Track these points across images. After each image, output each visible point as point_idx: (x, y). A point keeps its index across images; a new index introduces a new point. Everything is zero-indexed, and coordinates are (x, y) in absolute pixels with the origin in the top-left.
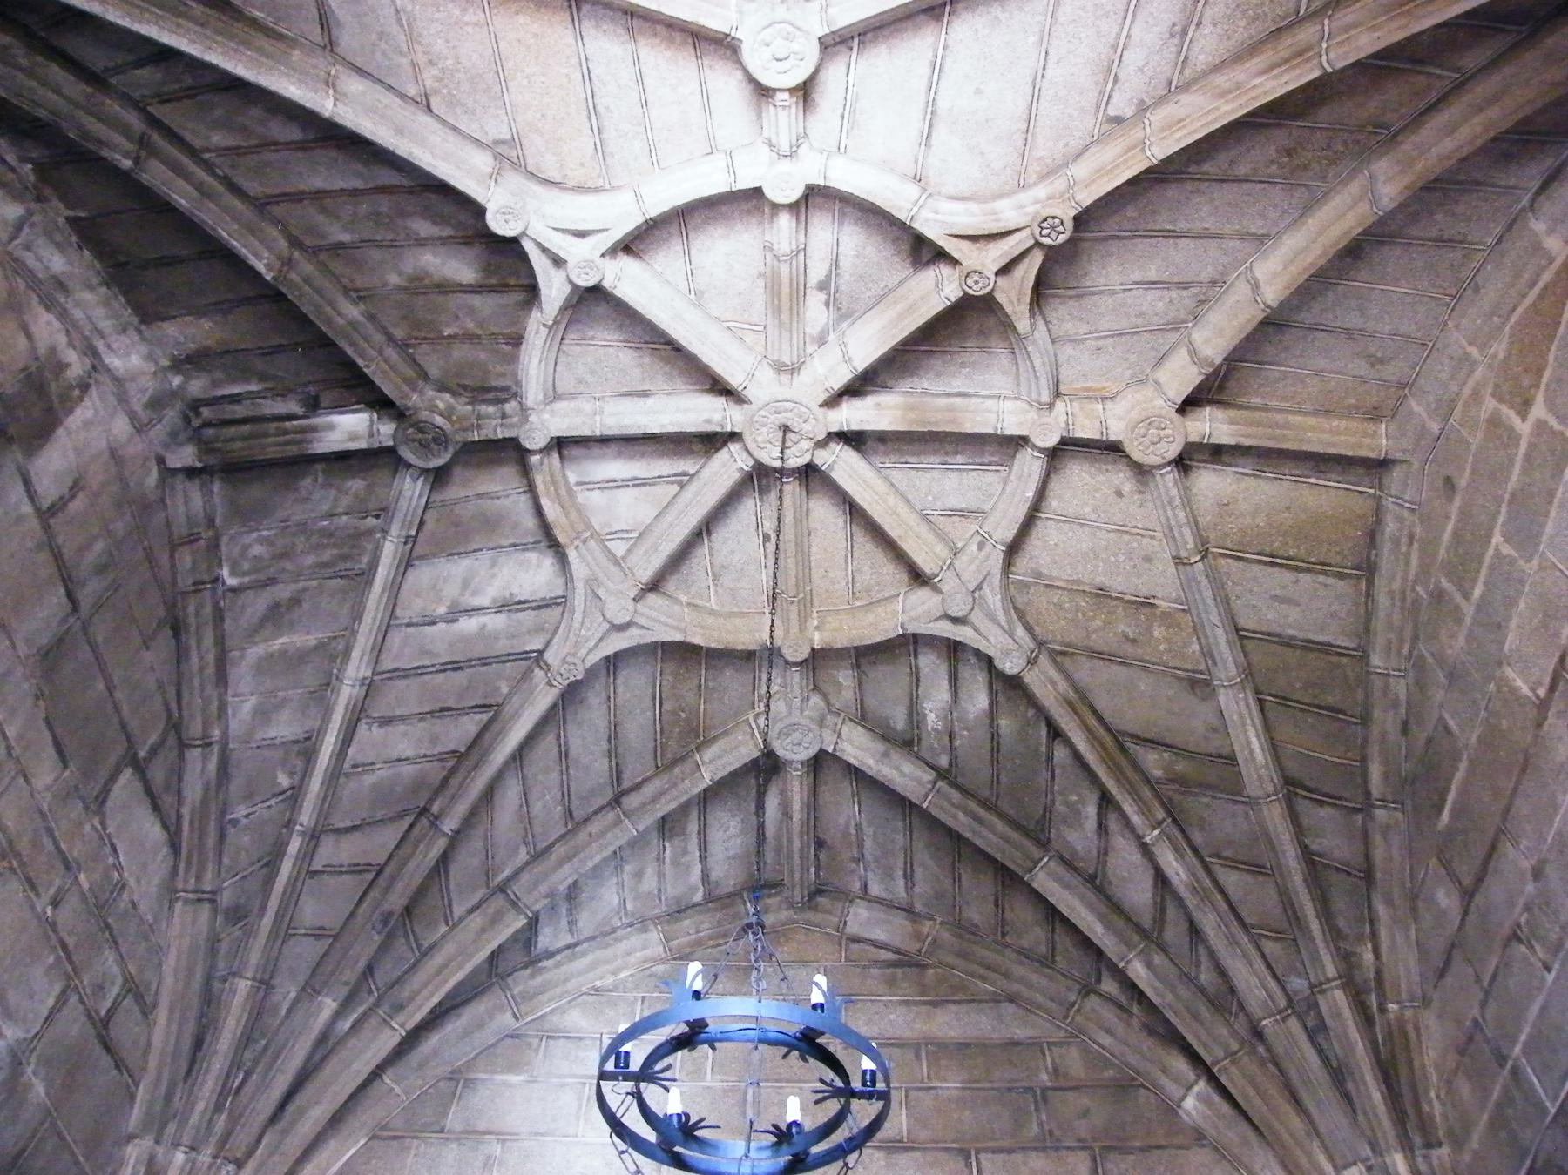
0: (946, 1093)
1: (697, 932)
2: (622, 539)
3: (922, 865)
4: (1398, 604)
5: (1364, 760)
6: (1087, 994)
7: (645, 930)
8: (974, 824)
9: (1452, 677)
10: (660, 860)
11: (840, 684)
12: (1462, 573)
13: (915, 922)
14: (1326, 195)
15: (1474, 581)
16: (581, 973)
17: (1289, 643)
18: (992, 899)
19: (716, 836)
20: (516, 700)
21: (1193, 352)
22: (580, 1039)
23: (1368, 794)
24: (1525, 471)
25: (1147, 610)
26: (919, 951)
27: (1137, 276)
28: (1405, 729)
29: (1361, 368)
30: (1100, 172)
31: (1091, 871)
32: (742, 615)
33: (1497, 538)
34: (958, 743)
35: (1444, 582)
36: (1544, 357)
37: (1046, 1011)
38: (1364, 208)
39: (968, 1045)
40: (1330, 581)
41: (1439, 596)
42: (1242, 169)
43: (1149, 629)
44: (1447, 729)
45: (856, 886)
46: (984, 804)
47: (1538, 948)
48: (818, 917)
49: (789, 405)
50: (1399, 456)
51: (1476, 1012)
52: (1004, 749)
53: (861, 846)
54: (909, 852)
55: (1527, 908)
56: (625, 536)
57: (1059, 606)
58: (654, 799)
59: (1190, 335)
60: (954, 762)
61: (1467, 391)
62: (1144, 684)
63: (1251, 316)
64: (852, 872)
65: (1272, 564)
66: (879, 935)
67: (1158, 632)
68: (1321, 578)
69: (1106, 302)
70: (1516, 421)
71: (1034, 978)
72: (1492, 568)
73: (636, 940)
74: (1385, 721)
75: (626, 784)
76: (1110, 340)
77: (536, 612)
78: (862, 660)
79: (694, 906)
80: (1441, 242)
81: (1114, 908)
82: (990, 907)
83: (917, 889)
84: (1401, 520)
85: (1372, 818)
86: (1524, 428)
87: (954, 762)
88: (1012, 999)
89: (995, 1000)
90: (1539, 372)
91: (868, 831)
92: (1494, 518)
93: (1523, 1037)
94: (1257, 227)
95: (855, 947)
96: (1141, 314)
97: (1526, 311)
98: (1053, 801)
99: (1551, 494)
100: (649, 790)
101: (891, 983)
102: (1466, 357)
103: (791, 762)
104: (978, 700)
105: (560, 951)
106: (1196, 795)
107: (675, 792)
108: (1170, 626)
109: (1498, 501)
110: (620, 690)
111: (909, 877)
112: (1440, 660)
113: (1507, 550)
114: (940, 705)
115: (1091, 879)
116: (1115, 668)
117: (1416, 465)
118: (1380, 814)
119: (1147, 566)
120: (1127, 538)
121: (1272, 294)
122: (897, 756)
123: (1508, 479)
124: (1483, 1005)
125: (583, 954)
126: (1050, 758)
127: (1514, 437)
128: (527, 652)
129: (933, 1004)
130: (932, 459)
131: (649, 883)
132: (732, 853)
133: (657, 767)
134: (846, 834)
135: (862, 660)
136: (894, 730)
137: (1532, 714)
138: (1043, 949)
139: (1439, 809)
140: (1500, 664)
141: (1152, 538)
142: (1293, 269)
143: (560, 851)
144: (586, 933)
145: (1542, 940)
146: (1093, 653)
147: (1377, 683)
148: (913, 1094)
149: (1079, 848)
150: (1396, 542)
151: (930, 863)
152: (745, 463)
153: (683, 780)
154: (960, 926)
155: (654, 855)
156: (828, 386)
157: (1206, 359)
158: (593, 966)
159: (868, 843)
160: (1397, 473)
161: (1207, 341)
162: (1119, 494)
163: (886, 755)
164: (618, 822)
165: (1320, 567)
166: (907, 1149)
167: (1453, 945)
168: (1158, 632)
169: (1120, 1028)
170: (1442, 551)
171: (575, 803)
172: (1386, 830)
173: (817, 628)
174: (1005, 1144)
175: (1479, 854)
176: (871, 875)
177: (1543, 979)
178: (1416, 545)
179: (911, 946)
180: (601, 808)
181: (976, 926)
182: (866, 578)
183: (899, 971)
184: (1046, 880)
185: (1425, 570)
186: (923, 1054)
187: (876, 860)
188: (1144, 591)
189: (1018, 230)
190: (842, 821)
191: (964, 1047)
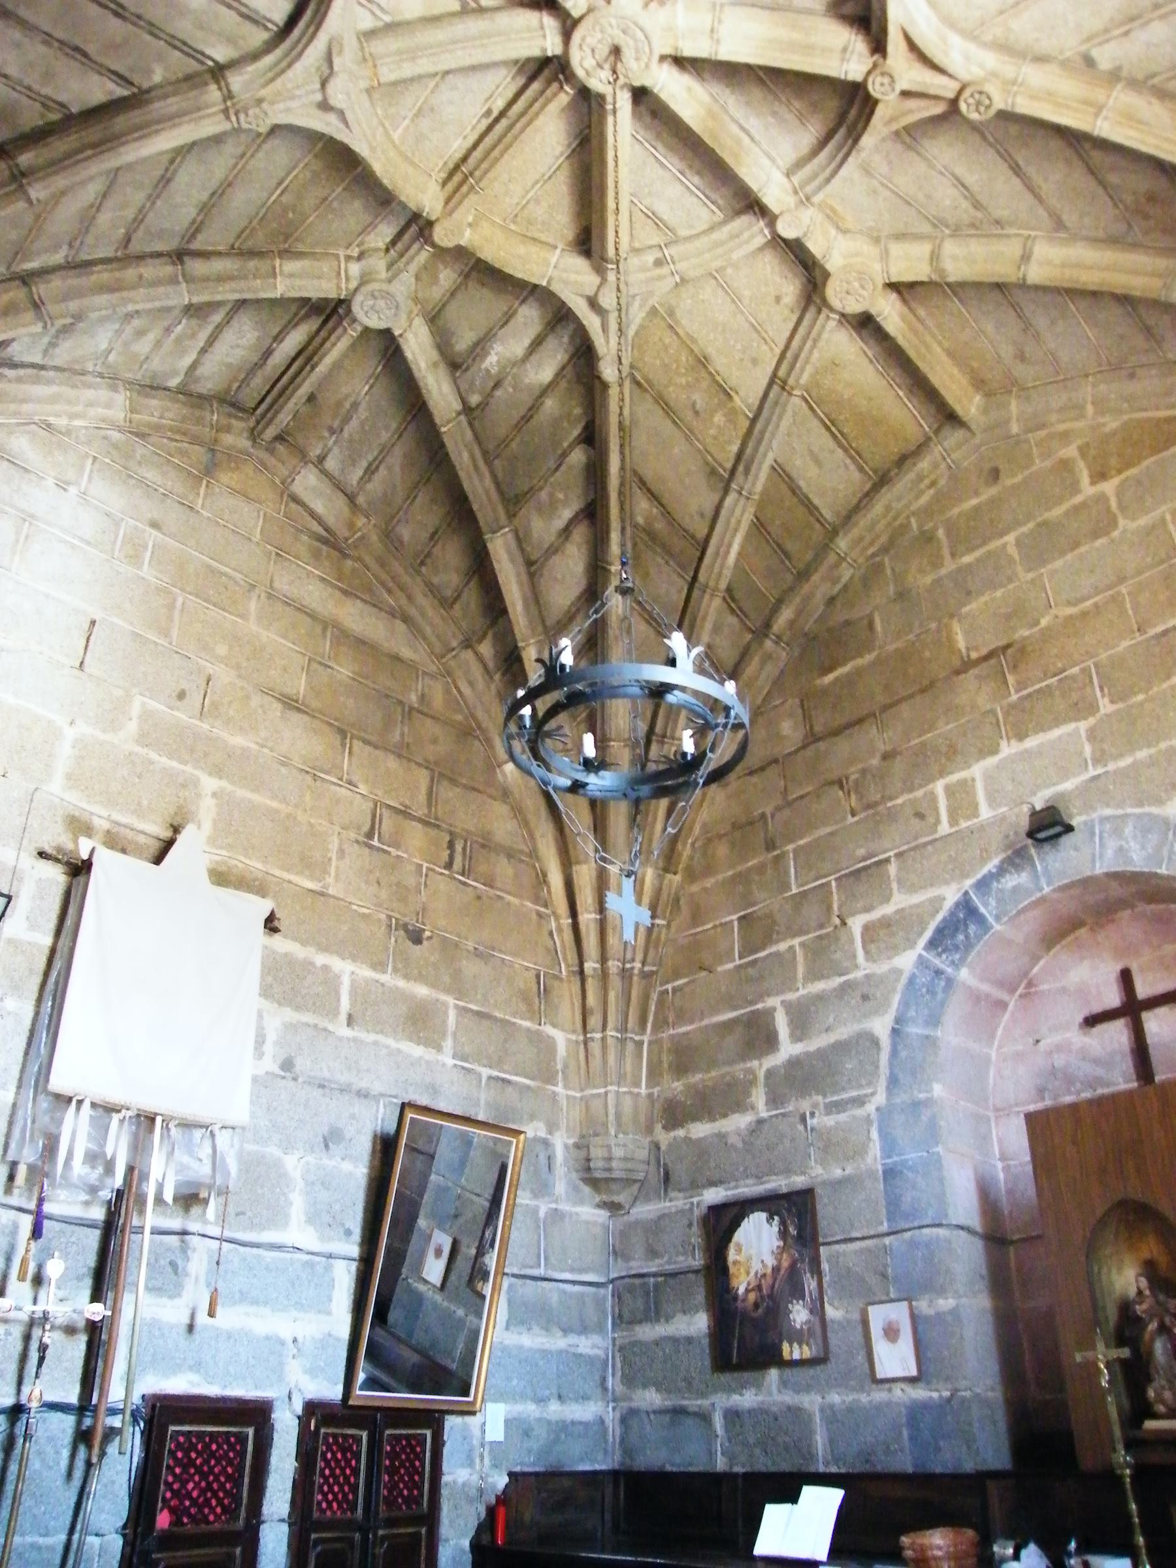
0: (339, 676)
1: (161, 417)
2: (373, 13)
3: (389, 469)
4: (889, 518)
5: (780, 602)
6: (467, 647)
7: (114, 389)
8: (471, 468)
9: (902, 595)
10: (168, 330)
11: (437, 278)
12: (962, 539)
13: (354, 513)
14: (1135, 246)
15: (971, 550)
16: (39, 400)
17: (794, 490)
18: (431, 530)
19: (229, 336)
20: (173, 104)
21: (935, 257)
22: (26, 470)
23: (767, 625)
24: (1067, 514)
25: (722, 396)
26: (347, 539)
27: (960, 171)
28: (831, 601)
29: (1007, 351)
30: (1049, 96)
31: (533, 558)
32: (413, 164)
33: (1010, 538)
34: (498, 393)
35: (941, 533)
36: (1140, 459)
37: (429, 645)
38: (1157, 283)
39: (363, 643)
40: (852, 467)
41: (928, 538)
42: (1113, 178)
43: (713, 412)
44: (871, 626)
45: (315, 452)
46: (485, 453)
47: (853, 797)
48: (271, 461)
49: (640, 35)
50: (973, 427)
51: (768, 810)
52: (533, 422)
53: (347, 420)
54: (385, 451)
55: (864, 772)
56: (378, 13)
57: (666, 348)
58: (221, 279)
59: (942, 240)
60: (483, 405)
61: (1061, 427)
62: (679, 448)
63: (1005, 271)
64: (323, 438)
65: (828, 428)
66: (319, 507)
67: (719, 418)
68: (848, 461)
69: (921, 167)
70: (1085, 479)
71: (430, 613)
72: (989, 554)
73: (104, 394)
74: (819, 587)
75: (195, 246)
76: (888, 193)
77: (239, 19)
78: (474, 274)
79: (166, 389)
80: (1148, 331)
81: (535, 598)
82: (425, 535)
83: (369, 486)
84: (936, 466)
85: (761, 644)
86: (1088, 489)
87: (483, 405)
88: (406, 619)
89: (392, 614)
90: (1128, 465)
91: (363, 413)
92: (1019, 524)
93: (801, 842)
94: (1070, 219)
95: (293, 505)
96: (928, 197)
97: (1148, 420)
98: (541, 489)
99: (1076, 545)
100: (218, 266)
101: (316, 555)
102: (1082, 407)
103: (354, 320)
104: (544, 370)
105: (23, 365)
106: (655, 552)
107: (242, 284)
108: (730, 421)
109: (1029, 517)
110: (260, 155)
111: (370, 471)
112: (898, 578)
113: (1012, 550)
114: (508, 354)
115: (529, 563)
116: (669, 423)
117: (977, 441)
118: (768, 644)
119: (750, 365)
120: (755, 335)
121: (1035, 274)
122: (443, 372)
123: (1048, 509)
124: (778, 809)
125: (49, 382)
126: (565, 455)
127: (1075, 488)
128: (203, 54)
129: (345, 593)
130: (676, 161)
131: (143, 347)
132: (230, 360)
133: (232, 247)
134: (339, 404)
135: (474, 274)
136: (452, 346)
137: (957, 663)
138: (449, 593)
139: (831, 669)
140: (952, 616)
141: (771, 349)
142: (1067, 273)
143: (102, 275)
144: (57, 362)
145: (861, 797)
146: (662, 401)
147: (832, 558)
148: (315, 666)
149: (535, 535)
150: (920, 478)
151: (397, 469)
152: (552, 45)
153: (255, 277)
154: (387, 536)
155: (166, 324)
156: (680, 44)
157: (944, 271)
158: (54, 399)
159: (354, 423)
160: (960, 434)
161: (955, 258)
162: (778, 299)
163: (435, 365)
164: (173, 281)
165: (855, 454)
166: (299, 710)
167: (776, 761)
168: (719, 418)
169: (481, 684)
170: (956, 511)
171: (140, 233)
172: (768, 657)
173: (470, 225)
174: (373, 739)
175: (840, 720)
176: (336, 450)
177: (844, 818)
178: (932, 491)
179: (342, 532)
180: (159, 255)
181: (402, 543)
182: (539, 212)
183: (324, 548)
184: (500, 548)
185: (927, 512)
186: (329, 634)
187: (351, 441)
188: (733, 382)
189: (950, 76)
190: (345, 390)
191: (361, 644)
